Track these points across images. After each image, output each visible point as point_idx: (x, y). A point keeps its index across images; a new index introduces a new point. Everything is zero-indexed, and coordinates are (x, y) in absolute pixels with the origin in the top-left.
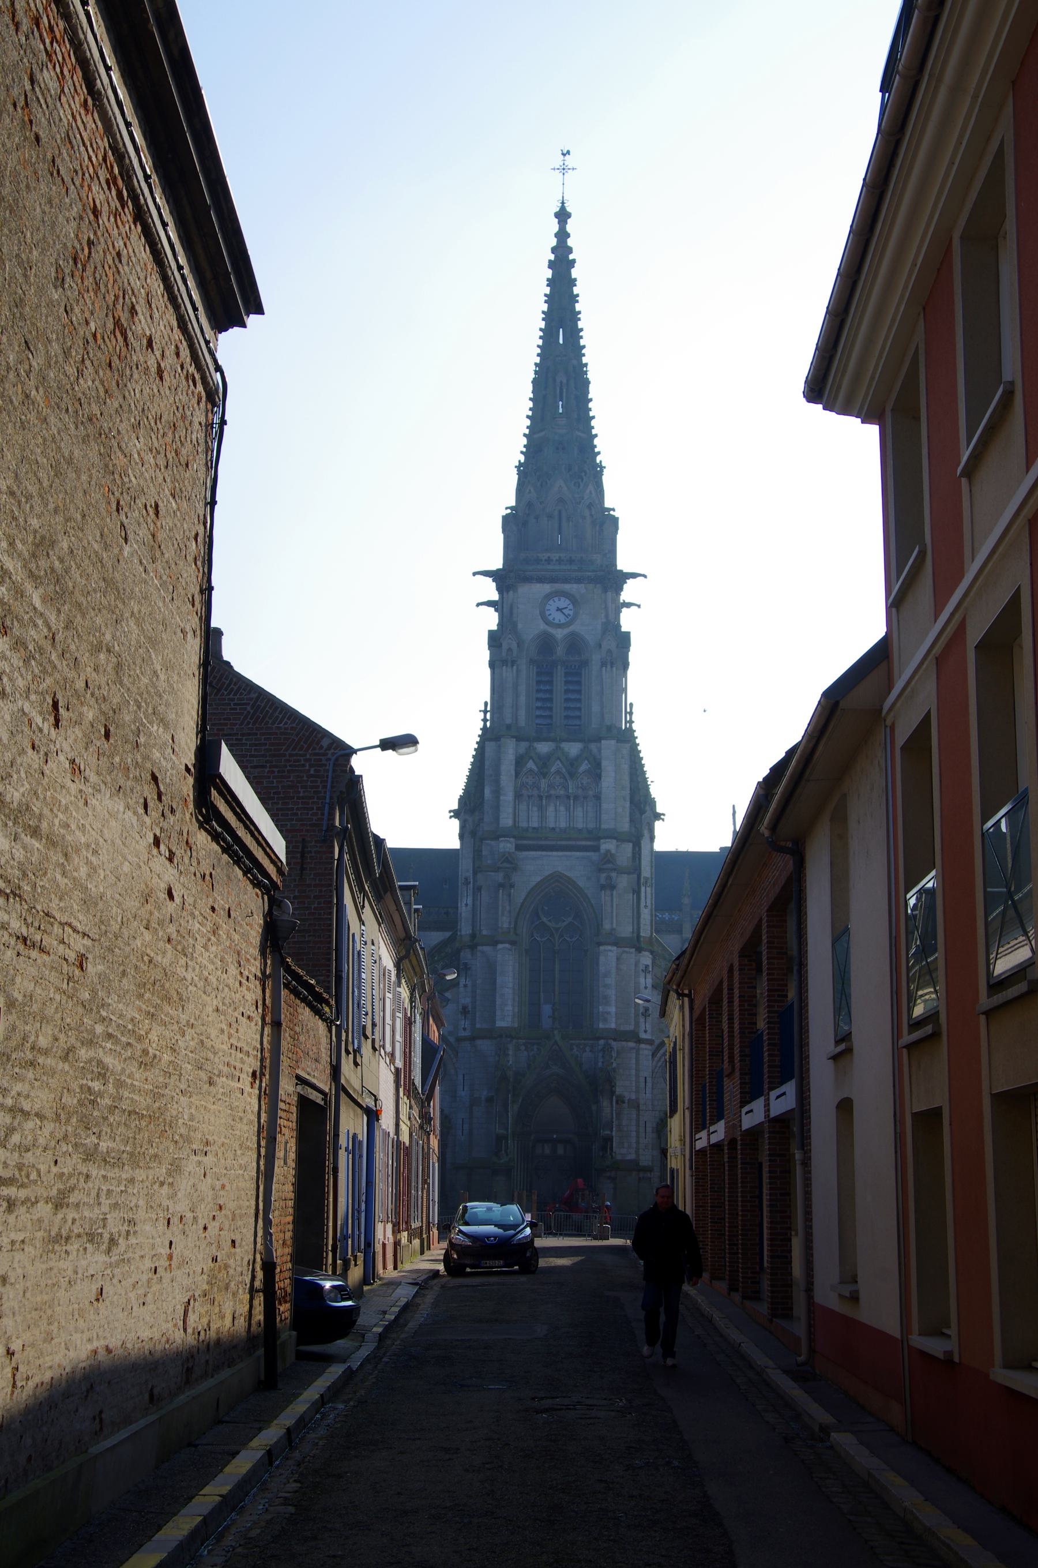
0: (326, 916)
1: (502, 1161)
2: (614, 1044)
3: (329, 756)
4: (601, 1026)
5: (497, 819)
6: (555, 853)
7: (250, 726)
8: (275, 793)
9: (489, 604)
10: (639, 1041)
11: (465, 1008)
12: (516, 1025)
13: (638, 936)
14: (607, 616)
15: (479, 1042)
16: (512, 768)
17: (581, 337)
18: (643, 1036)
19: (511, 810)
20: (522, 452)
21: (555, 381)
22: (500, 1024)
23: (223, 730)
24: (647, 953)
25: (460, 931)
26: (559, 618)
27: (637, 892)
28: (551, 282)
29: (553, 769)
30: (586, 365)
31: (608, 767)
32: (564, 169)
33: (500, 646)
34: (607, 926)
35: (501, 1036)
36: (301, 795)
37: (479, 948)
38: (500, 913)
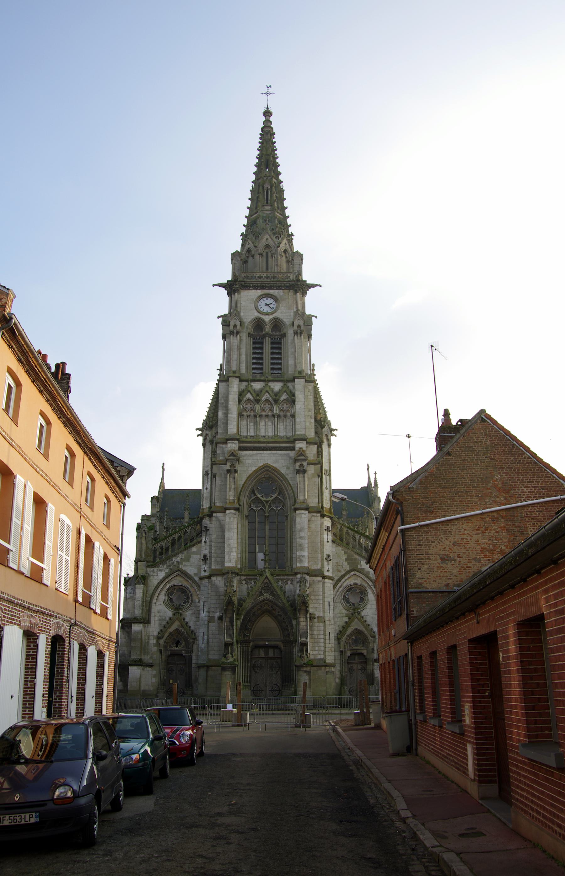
1: (229, 661)
2: (307, 577)
4: (298, 565)
5: (226, 430)
6: (265, 452)
10: (324, 577)
11: (205, 557)
12: (239, 566)
13: (322, 507)
14: (297, 308)
15: (213, 578)
16: (237, 396)
18: (326, 574)
19: (235, 423)
21: (263, 187)
22: (227, 564)
24: (328, 519)
25: (203, 506)
26: (267, 309)
29: (263, 399)
31: (299, 396)
32: (268, 94)
33: (229, 325)
34: (301, 498)
35: (228, 573)
38: (228, 489)
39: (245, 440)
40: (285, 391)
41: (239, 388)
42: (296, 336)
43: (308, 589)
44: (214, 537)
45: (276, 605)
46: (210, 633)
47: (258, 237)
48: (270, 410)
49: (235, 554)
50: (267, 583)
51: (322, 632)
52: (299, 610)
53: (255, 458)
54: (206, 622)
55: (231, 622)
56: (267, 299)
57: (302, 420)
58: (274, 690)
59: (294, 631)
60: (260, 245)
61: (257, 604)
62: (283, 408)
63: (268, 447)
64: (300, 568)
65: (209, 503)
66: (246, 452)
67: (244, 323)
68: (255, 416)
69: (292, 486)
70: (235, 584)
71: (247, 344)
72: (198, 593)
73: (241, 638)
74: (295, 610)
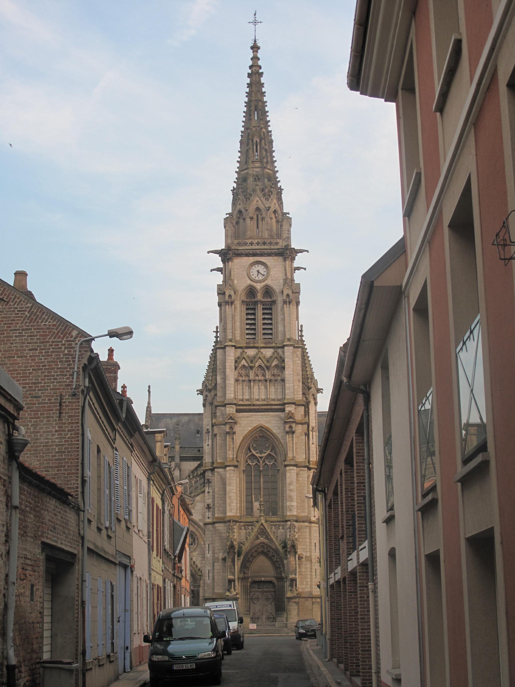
0: (75, 443)
2: (296, 524)
3: (77, 342)
4: (288, 514)
6: (259, 413)
7: (27, 324)
8: (43, 366)
9: (219, 270)
10: (311, 522)
11: (208, 505)
12: (238, 515)
16: (233, 364)
17: (268, 116)
19: (233, 389)
20: (235, 182)
21: (253, 141)
22: (228, 514)
23: (10, 327)
25: (205, 460)
27: (307, 435)
28: (249, 85)
29: (257, 365)
30: (271, 131)
31: (289, 363)
32: (255, 23)
34: (290, 455)
36: (59, 366)
37: (216, 470)
39: (241, 403)
40: (276, 358)
41: (235, 355)
42: (285, 305)
43: (297, 533)
44: (216, 490)
45: (270, 547)
46: (216, 571)
47: (249, 199)
48: (263, 375)
49: (235, 505)
50: (262, 529)
51: (309, 570)
52: (289, 552)
53: (250, 419)
54: (211, 562)
55: (233, 561)
56: (258, 266)
57: (291, 385)
58: (269, 618)
59: (286, 569)
60: (251, 208)
61: (254, 547)
62: (274, 373)
63: (262, 409)
64: (290, 516)
65: (211, 458)
66: (243, 414)
67: (237, 290)
68: (250, 381)
69: (283, 443)
70: (235, 531)
71: (241, 311)
72: (203, 536)
73: (241, 576)
74: (286, 551)
